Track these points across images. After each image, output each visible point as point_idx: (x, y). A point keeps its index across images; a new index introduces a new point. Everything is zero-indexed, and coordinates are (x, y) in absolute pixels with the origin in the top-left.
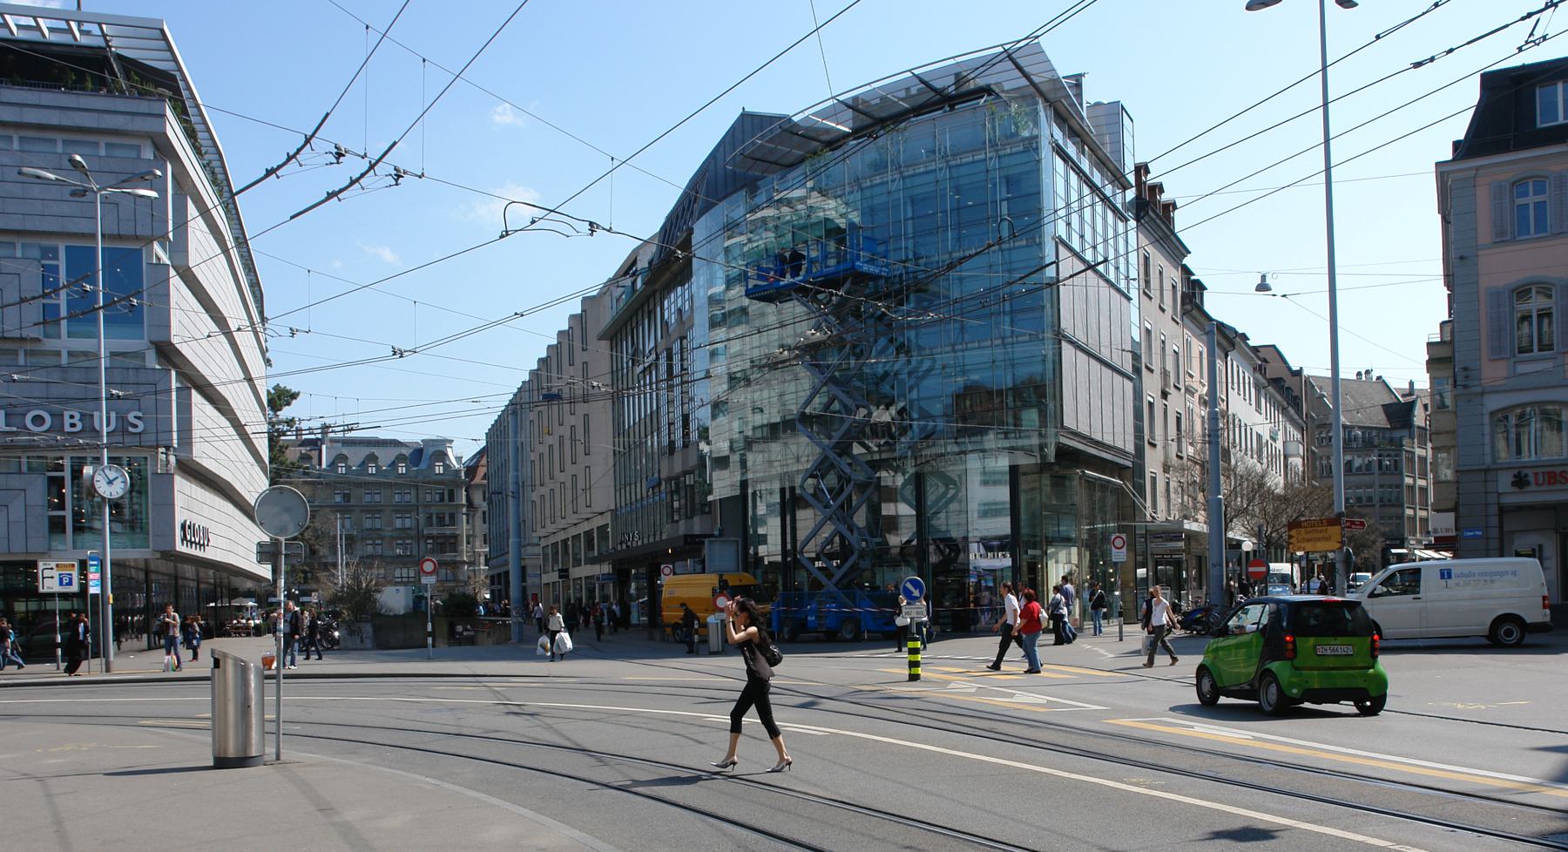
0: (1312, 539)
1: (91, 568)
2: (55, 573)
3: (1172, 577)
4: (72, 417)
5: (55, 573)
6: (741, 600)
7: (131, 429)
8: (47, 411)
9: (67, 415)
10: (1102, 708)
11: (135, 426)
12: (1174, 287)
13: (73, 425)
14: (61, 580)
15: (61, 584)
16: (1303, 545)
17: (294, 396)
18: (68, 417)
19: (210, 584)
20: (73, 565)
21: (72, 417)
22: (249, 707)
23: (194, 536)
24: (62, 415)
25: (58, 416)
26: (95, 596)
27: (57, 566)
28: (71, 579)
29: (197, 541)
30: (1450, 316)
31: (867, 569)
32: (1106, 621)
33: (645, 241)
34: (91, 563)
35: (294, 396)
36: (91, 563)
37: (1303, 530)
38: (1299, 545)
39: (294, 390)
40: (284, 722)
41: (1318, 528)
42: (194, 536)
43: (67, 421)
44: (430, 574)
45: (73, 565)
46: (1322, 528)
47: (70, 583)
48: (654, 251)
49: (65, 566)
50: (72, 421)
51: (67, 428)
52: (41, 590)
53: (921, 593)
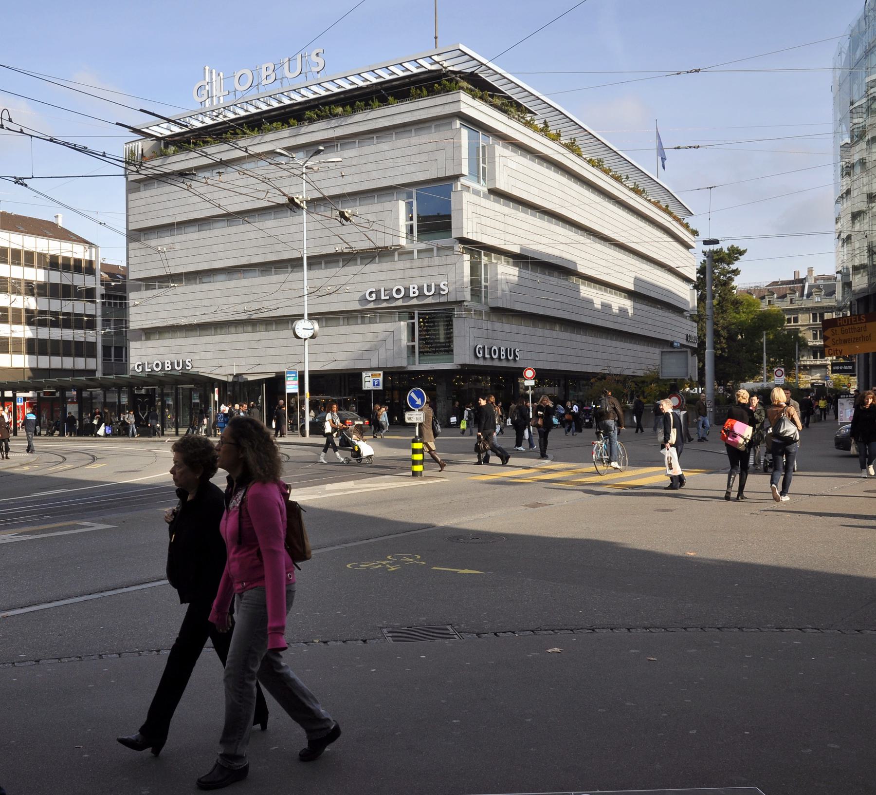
0: (849, 340)
1: (289, 379)
2: (371, 379)
3: (75, 396)
4: (414, 288)
5: (371, 379)
6: (516, 406)
10: (479, 572)
11: (444, 290)
13: (414, 293)
14: (374, 383)
15: (374, 385)
16: (839, 348)
17: (741, 253)
20: (380, 374)
21: (414, 288)
26: (292, 395)
27: (372, 375)
28: (378, 382)
33: (324, 196)
34: (288, 375)
35: (741, 253)
36: (288, 375)
37: (838, 329)
38: (835, 348)
39: (742, 249)
41: (856, 326)
43: (412, 290)
44: (530, 379)
45: (380, 374)
46: (860, 326)
47: (378, 385)
49: (376, 375)
50: (414, 290)
51: (412, 295)
52: (364, 389)
53: (423, 401)
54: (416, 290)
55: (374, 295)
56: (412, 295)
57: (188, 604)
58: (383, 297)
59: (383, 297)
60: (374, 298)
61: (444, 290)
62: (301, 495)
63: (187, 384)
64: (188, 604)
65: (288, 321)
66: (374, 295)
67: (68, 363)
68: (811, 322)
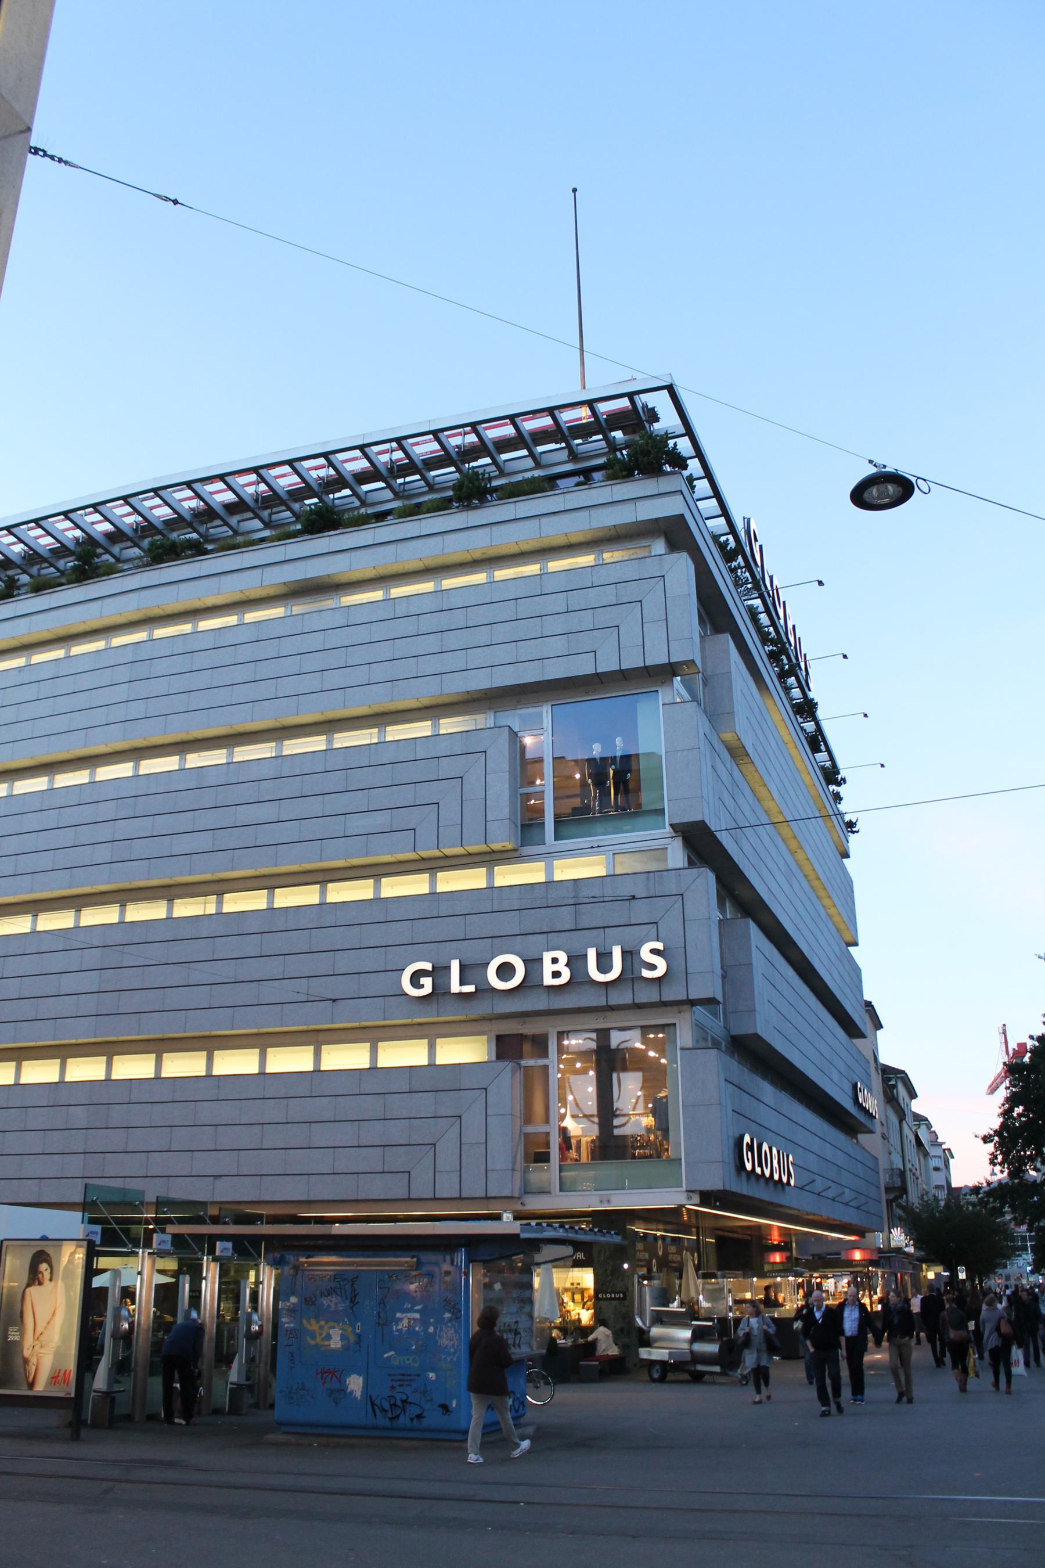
7: (646, 973)
8: (516, 954)
9: (547, 957)
11: (653, 967)
12: (910, 1142)
13: (556, 974)
18: (550, 961)
19: (902, 1358)
21: (555, 961)
22: (587, 693)
23: (760, 1165)
24: (540, 960)
25: (533, 964)
29: (767, 1173)
30: (248, 1379)
31: (993, 1170)
32: (168, 1246)
40: (682, 1049)
42: (760, 1165)
43: (548, 968)
48: (610, 1353)
50: (556, 967)
51: (548, 980)
54: (561, 966)
55: (427, 982)
56: (548, 980)
57: (643, 969)
58: (455, 987)
59: (455, 987)
60: (427, 989)
61: (654, 951)
62: (824, 871)
63: (1034, 1502)
64: (643, 969)
65: (518, 1503)
66: (427, 982)
67: (343, 1268)
68: (590, 1161)
